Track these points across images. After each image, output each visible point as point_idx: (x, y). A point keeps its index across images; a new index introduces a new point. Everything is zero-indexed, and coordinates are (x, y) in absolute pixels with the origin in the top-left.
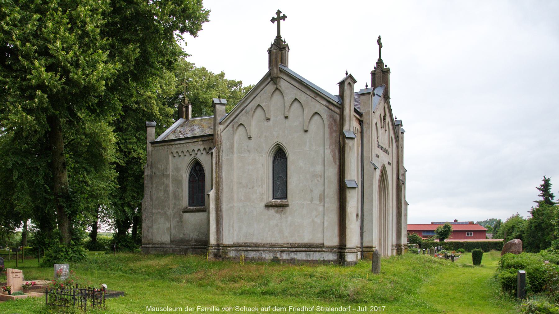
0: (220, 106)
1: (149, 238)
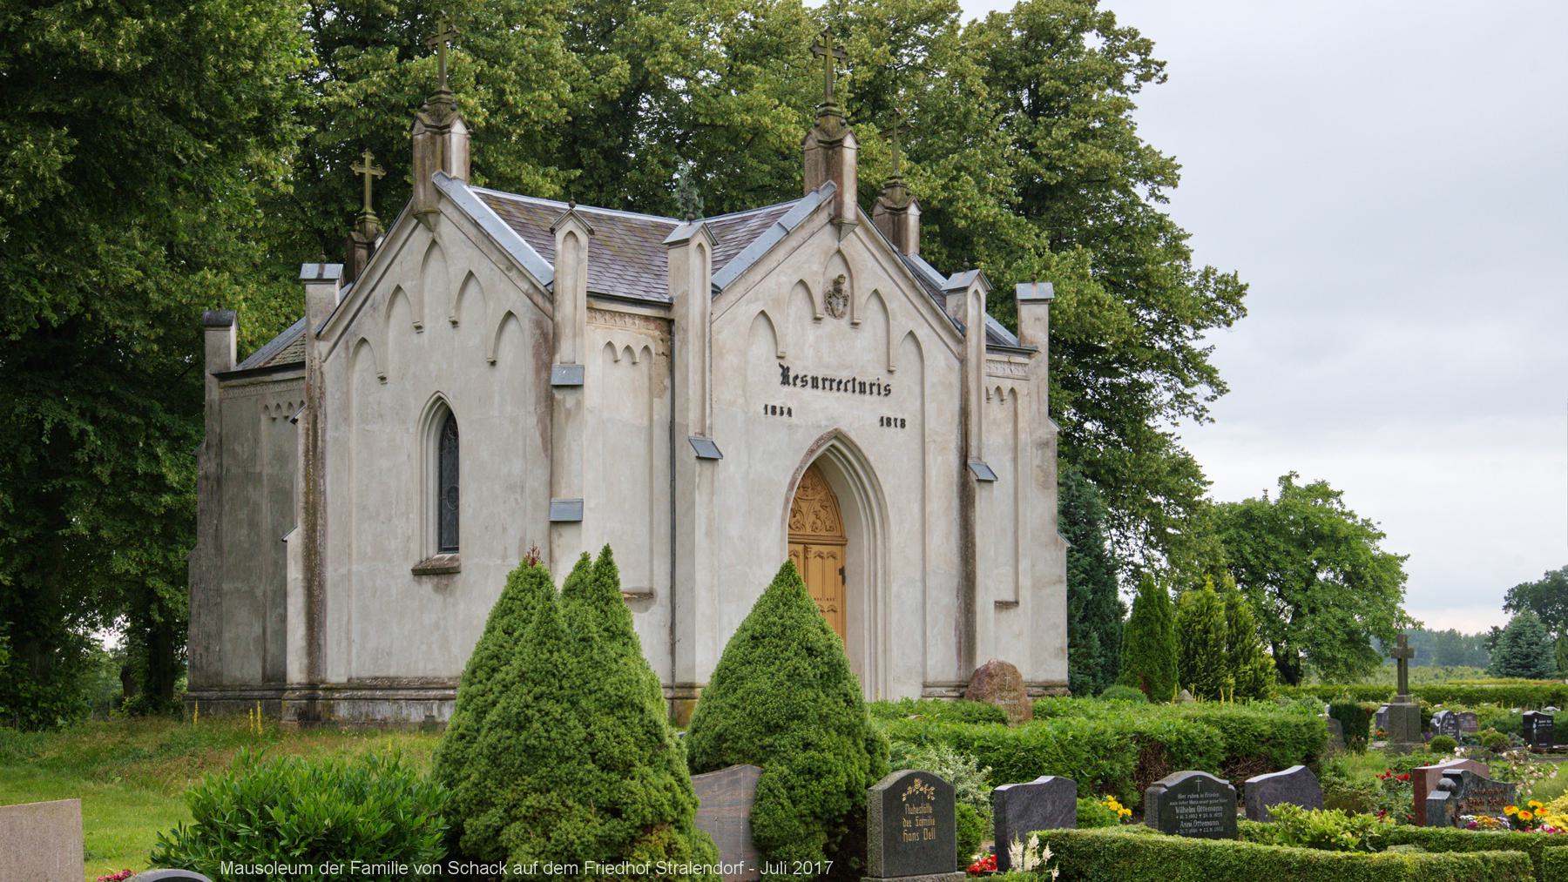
0: (320, 287)
1: (212, 669)
